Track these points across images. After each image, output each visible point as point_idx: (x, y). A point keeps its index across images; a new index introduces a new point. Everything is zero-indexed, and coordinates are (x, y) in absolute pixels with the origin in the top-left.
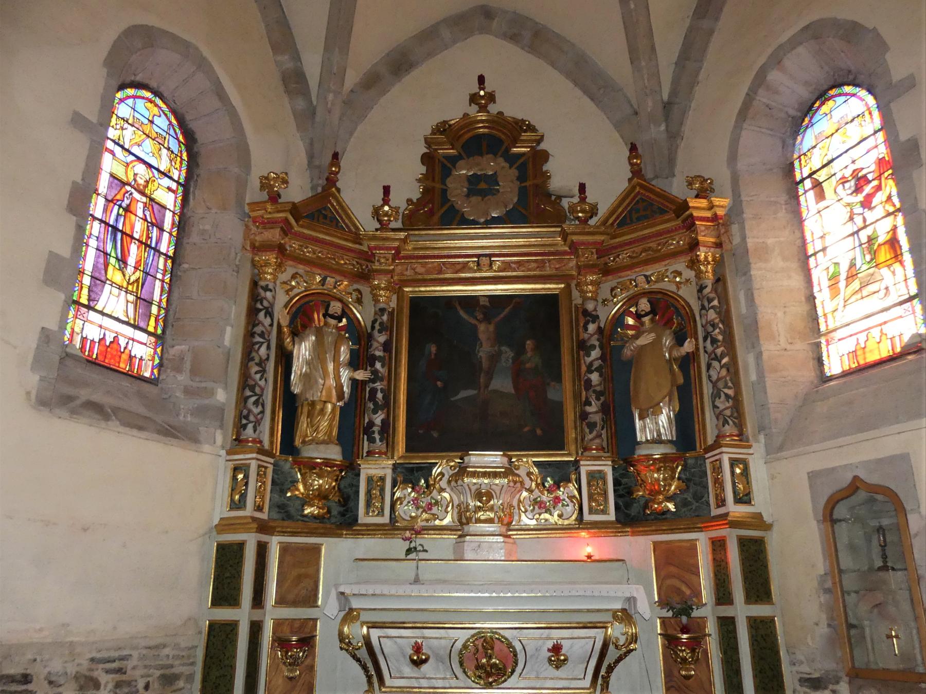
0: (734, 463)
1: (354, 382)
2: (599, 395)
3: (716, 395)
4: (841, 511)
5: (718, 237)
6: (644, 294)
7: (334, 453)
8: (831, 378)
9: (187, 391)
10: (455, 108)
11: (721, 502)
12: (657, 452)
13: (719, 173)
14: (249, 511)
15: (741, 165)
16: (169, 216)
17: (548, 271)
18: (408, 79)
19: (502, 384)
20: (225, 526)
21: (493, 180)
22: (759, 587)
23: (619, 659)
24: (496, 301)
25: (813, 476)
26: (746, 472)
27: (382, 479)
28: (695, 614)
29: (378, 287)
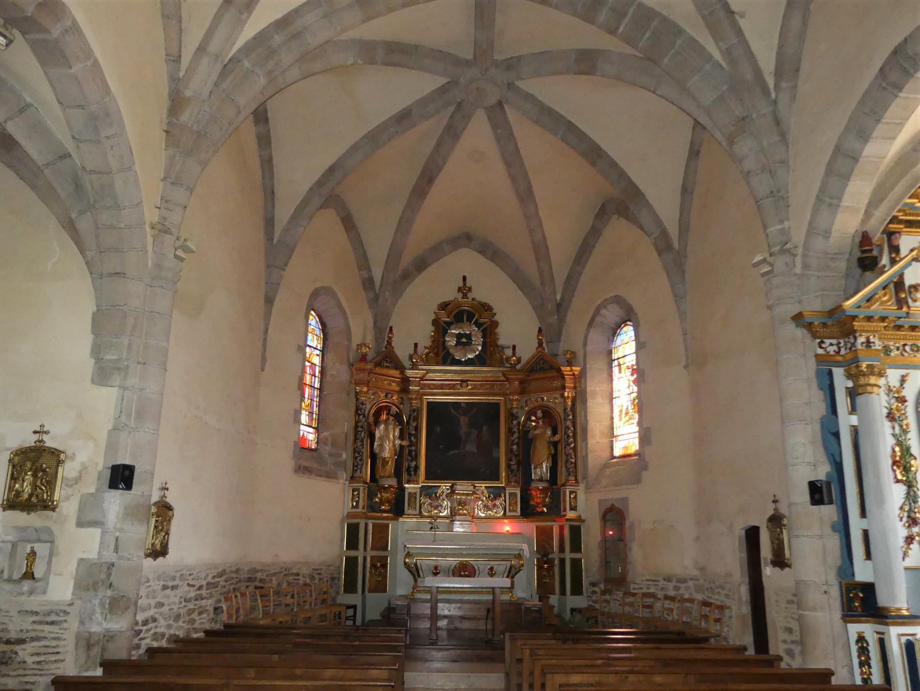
0: (571, 493)
1: (401, 446)
2: (516, 456)
3: (567, 461)
4: (608, 516)
5: (575, 383)
6: (539, 407)
7: (393, 482)
8: (615, 458)
9: (331, 455)
10: (450, 294)
11: (565, 510)
12: (541, 486)
13: (579, 349)
14: (360, 509)
15: (589, 348)
16: (317, 368)
17: (496, 390)
18: (426, 273)
19: (471, 447)
20: (350, 515)
21: (469, 337)
22: (576, 546)
23: (516, 573)
24: (470, 405)
25: (600, 501)
26: (575, 497)
27: (415, 494)
28: (550, 556)
29: (412, 399)
